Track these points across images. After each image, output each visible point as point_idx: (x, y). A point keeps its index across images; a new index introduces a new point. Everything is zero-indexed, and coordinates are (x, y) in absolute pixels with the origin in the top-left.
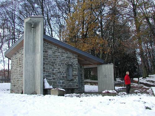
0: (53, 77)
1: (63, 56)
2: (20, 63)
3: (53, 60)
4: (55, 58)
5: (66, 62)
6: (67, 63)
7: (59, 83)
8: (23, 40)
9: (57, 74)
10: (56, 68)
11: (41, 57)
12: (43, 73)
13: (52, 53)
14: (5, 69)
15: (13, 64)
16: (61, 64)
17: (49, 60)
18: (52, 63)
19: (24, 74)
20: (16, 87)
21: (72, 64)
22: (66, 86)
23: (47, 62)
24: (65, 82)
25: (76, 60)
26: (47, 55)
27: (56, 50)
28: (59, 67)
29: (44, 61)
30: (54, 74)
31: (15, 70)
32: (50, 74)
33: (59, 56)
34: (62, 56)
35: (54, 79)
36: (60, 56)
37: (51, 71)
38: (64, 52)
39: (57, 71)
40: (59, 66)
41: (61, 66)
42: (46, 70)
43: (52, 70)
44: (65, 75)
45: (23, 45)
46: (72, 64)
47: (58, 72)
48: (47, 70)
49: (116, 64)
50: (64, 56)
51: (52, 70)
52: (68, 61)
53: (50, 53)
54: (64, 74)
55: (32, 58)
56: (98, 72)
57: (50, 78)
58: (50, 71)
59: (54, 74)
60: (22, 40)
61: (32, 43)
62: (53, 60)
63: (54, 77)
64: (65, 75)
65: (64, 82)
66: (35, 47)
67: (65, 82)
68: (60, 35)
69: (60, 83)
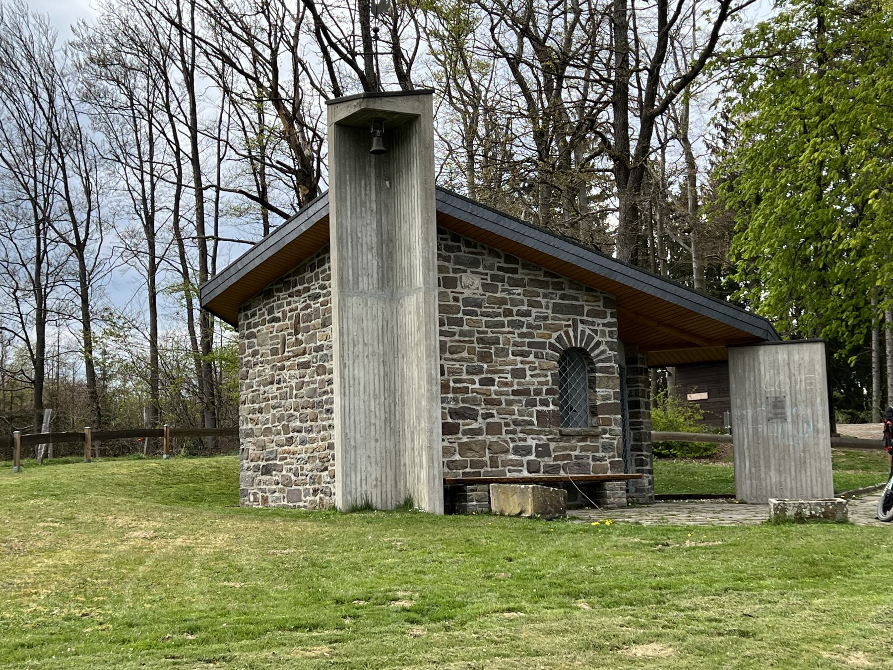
0: (490, 420)
1: (539, 305)
2: (298, 342)
3: (487, 325)
4: (499, 315)
5: (555, 335)
6: (559, 339)
7: (517, 450)
8: (327, 216)
9: (509, 403)
10: (502, 371)
11: (428, 315)
12: (439, 396)
13: (481, 291)
14: (76, 380)
15: (255, 354)
16: (530, 345)
17: (466, 328)
18: (481, 341)
19: (337, 406)
20: (276, 476)
21: (587, 344)
22: (555, 469)
23: (457, 338)
24: (552, 445)
25: (609, 319)
26: (456, 299)
27: (499, 268)
28: (520, 366)
29: (442, 333)
30: (489, 402)
31: (272, 383)
32: (474, 401)
33: (514, 303)
34: (531, 304)
35: (494, 429)
36: (522, 303)
37: (477, 386)
38: (542, 278)
39: (506, 384)
40: (519, 359)
41: (531, 358)
42: (452, 384)
43: (483, 382)
44: (552, 407)
45: (327, 249)
46: (587, 344)
47: (515, 393)
48: (455, 382)
49: (832, 346)
50: (543, 301)
51: (483, 382)
52: (567, 333)
53: (467, 293)
54: (545, 403)
55: (374, 318)
56: (733, 386)
57: (475, 426)
58: (471, 386)
59: (489, 402)
60: (315, 220)
61: (374, 239)
62: (487, 325)
63: (496, 419)
64: (552, 407)
65: (546, 447)
66: (391, 256)
67: (552, 445)
68: (886, 590)
69: (527, 451)
